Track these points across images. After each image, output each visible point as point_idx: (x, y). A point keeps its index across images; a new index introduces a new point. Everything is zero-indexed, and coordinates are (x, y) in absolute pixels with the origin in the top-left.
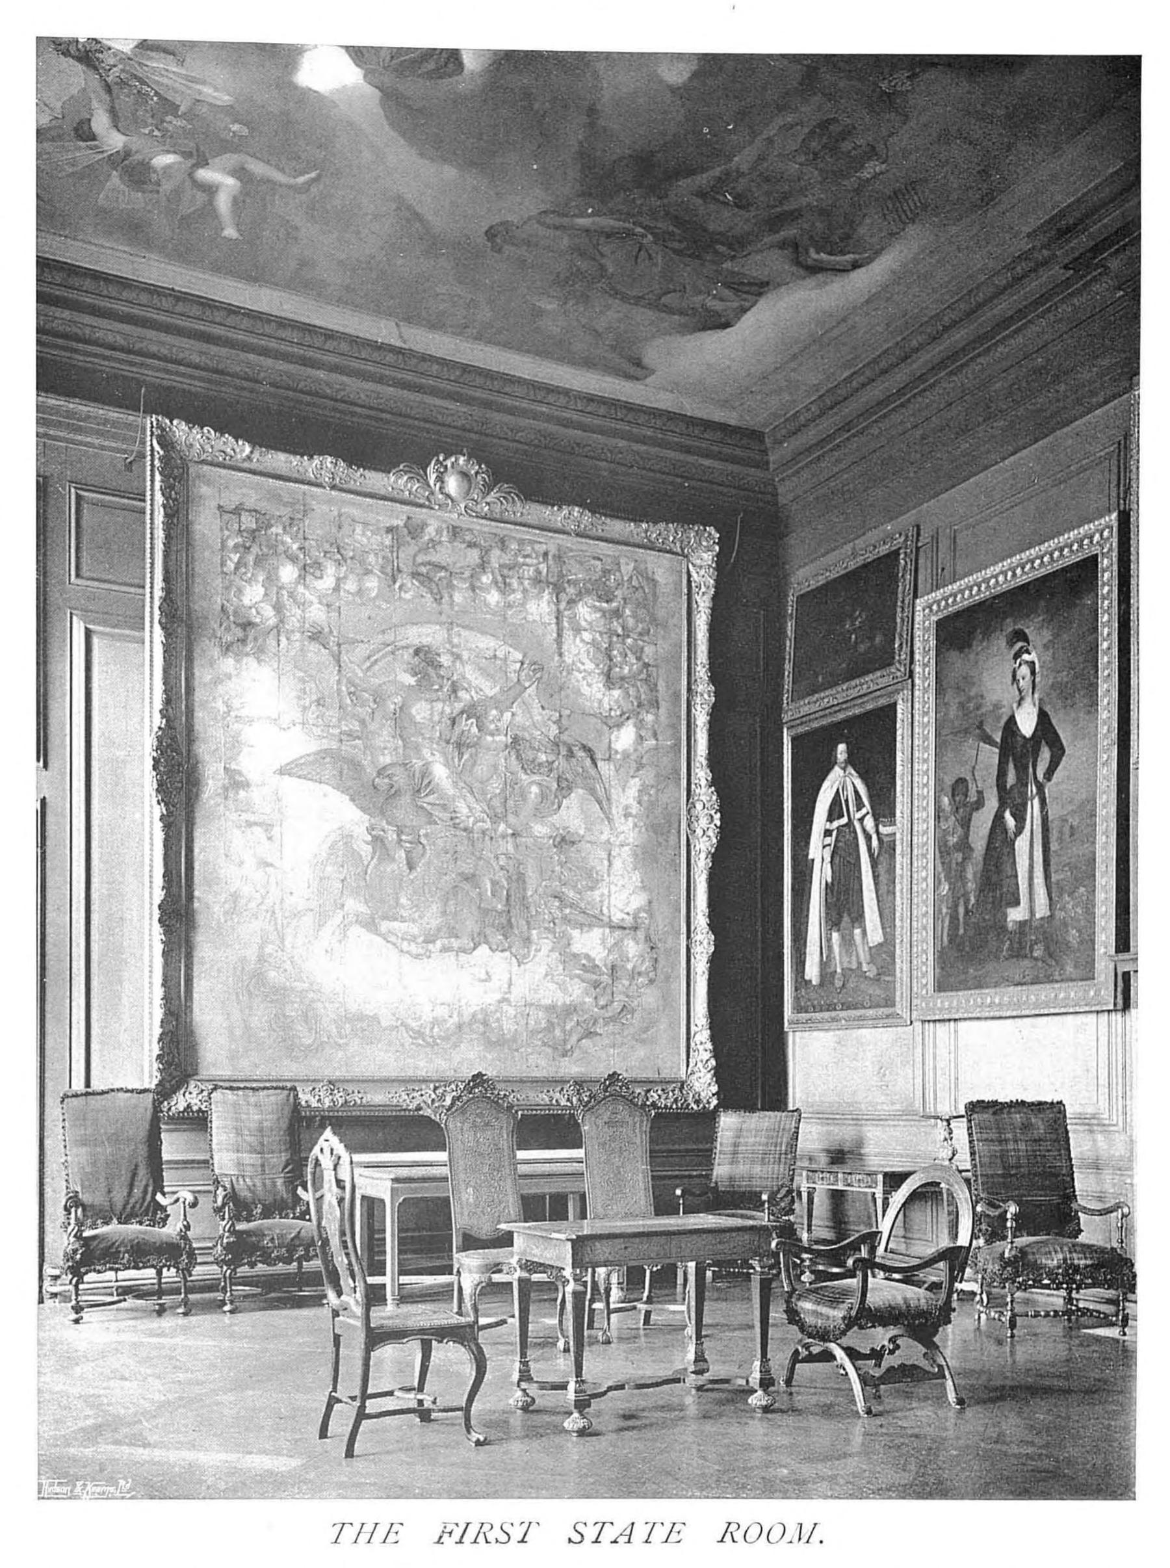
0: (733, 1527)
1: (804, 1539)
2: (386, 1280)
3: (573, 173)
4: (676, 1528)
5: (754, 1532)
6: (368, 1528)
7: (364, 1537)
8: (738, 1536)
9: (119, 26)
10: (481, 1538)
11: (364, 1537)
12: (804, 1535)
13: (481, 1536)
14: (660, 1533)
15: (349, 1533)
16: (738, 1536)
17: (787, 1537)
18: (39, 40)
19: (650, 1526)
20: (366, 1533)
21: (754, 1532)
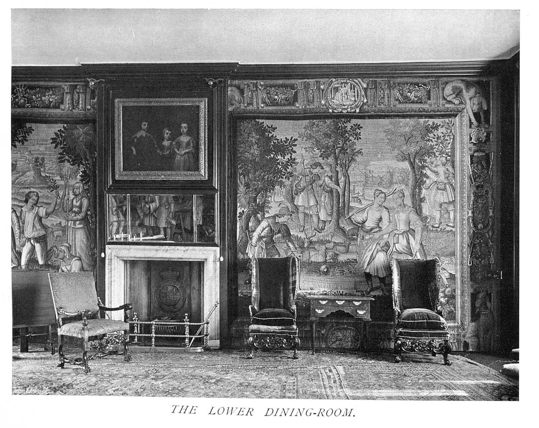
0: (322, 411)
1: (348, 415)
2: (154, 335)
3: (32, 137)
4: (194, 408)
5: (338, 412)
6: (185, 408)
7: (183, 411)
8: (324, 414)
9: (14, 8)
10: (320, 414)
11: (183, 411)
12: (348, 413)
13: (321, 414)
14: (178, 409)
15: (178, 409)
16: (324, 414)
17: (342, 414)
18: (516, 13)
19: (174, 407)
20: (184, 410)
21: (338, 412)
